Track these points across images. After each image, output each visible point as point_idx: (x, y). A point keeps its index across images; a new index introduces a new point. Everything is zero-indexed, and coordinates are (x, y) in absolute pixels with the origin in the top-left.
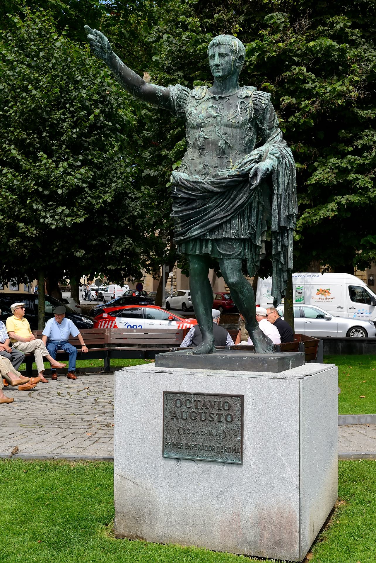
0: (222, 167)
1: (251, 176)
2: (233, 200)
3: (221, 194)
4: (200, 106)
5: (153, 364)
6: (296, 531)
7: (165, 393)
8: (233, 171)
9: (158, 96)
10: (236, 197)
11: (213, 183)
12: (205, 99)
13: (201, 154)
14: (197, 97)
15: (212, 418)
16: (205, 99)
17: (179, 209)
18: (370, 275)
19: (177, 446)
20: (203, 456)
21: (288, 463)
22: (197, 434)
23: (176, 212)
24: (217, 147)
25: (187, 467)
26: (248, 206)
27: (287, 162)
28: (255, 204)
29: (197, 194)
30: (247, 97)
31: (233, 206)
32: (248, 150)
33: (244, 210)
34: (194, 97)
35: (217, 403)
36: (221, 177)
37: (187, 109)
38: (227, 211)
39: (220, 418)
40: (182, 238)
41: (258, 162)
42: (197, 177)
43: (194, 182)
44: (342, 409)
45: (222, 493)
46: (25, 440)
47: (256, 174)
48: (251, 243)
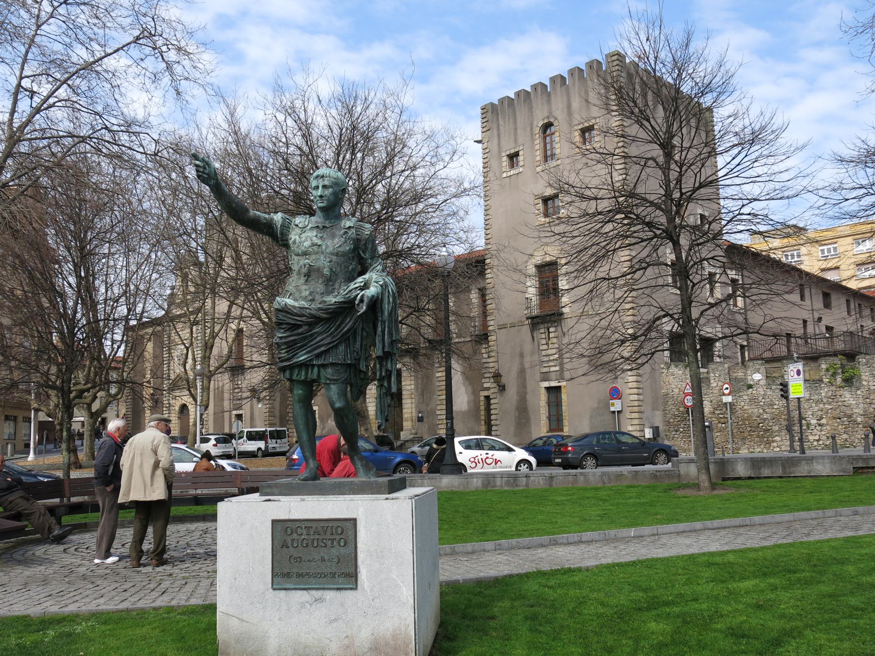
0: (328, 293)
1: (357, 302)
2: (339, 326)
3: (327, 320)
4: (304, 235)
5: (258, 494)
6: (412, 651)
7: (274, 522)
8: (339, 299)
9: (262, 224)
10: (342, 323)
11: (320, 309)
12: (308, 228)
13: (307, 281)
14: (300, 226)
15: (324, 543)
16: (308, 228)
17: (285, 335)
18: (420, 412)
19: (288, 575)
20: (315, 584)
21: (403, 582)
22: (309, 561)
23: (281, 338)
24: (323, 275)
25: (300, 596)
26: (353, 331)
27: (390, 290)
28: (359, 331)
29: (304, 319)
30: (350, 227)
31: (340, 332)
32: (352, 279)
33: (349, 337)
34: (297, 225)
35: (329, 529)
36: (328, 303)
37: (290, 237)
38: (334, 337)
39: (332, 543)
40: (288, 364)
41: (363, 290)
42: (305, 304)
43: (300, 308)
44: (216, 604)
45: (335, 620)
46: (80, 596)
47: (362, 301)
48: (356, 368)
